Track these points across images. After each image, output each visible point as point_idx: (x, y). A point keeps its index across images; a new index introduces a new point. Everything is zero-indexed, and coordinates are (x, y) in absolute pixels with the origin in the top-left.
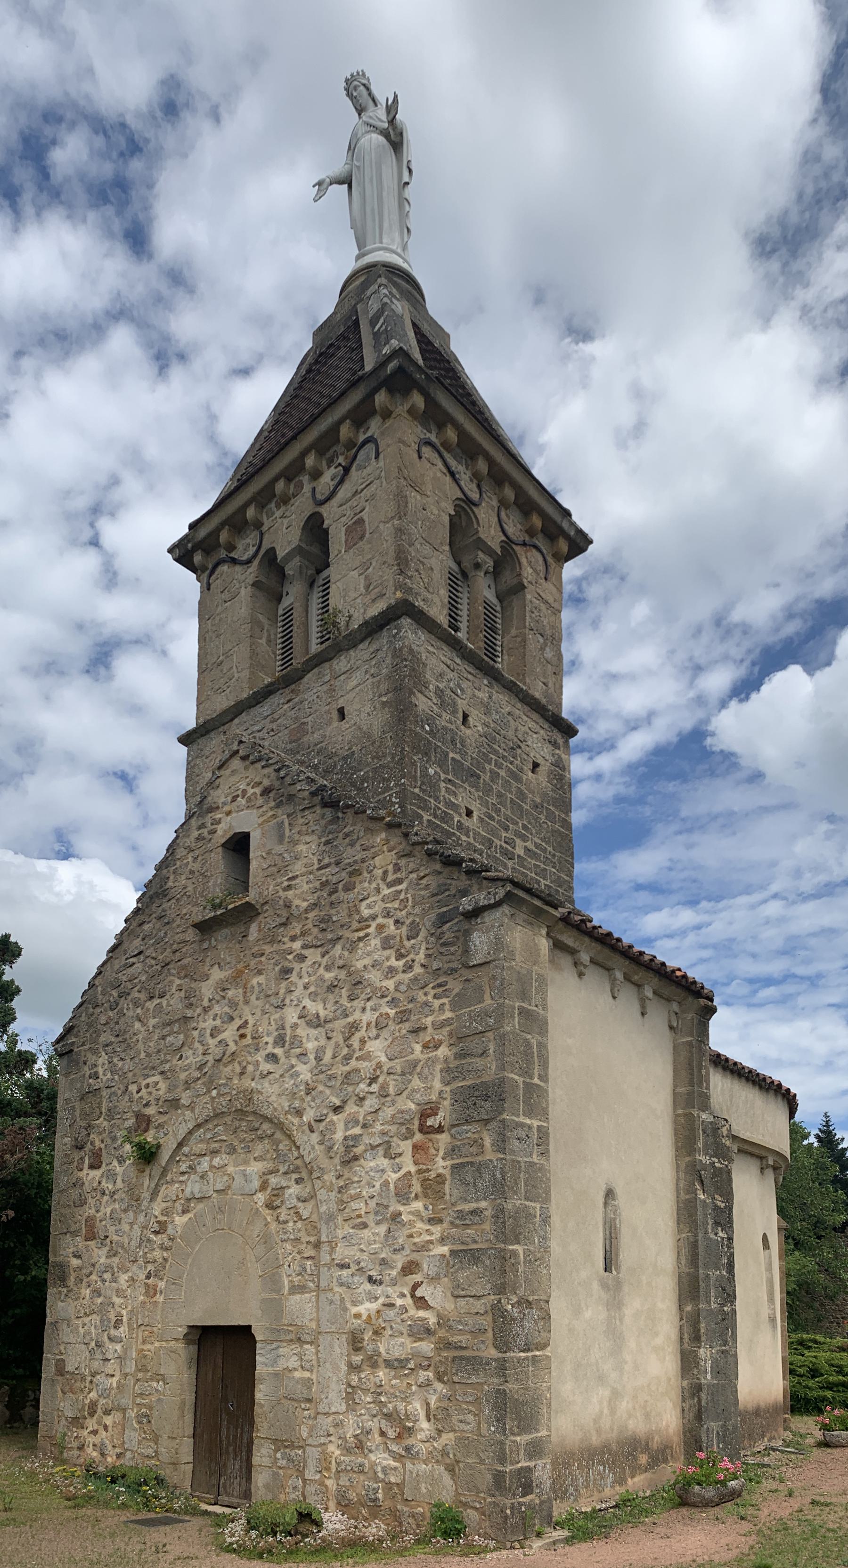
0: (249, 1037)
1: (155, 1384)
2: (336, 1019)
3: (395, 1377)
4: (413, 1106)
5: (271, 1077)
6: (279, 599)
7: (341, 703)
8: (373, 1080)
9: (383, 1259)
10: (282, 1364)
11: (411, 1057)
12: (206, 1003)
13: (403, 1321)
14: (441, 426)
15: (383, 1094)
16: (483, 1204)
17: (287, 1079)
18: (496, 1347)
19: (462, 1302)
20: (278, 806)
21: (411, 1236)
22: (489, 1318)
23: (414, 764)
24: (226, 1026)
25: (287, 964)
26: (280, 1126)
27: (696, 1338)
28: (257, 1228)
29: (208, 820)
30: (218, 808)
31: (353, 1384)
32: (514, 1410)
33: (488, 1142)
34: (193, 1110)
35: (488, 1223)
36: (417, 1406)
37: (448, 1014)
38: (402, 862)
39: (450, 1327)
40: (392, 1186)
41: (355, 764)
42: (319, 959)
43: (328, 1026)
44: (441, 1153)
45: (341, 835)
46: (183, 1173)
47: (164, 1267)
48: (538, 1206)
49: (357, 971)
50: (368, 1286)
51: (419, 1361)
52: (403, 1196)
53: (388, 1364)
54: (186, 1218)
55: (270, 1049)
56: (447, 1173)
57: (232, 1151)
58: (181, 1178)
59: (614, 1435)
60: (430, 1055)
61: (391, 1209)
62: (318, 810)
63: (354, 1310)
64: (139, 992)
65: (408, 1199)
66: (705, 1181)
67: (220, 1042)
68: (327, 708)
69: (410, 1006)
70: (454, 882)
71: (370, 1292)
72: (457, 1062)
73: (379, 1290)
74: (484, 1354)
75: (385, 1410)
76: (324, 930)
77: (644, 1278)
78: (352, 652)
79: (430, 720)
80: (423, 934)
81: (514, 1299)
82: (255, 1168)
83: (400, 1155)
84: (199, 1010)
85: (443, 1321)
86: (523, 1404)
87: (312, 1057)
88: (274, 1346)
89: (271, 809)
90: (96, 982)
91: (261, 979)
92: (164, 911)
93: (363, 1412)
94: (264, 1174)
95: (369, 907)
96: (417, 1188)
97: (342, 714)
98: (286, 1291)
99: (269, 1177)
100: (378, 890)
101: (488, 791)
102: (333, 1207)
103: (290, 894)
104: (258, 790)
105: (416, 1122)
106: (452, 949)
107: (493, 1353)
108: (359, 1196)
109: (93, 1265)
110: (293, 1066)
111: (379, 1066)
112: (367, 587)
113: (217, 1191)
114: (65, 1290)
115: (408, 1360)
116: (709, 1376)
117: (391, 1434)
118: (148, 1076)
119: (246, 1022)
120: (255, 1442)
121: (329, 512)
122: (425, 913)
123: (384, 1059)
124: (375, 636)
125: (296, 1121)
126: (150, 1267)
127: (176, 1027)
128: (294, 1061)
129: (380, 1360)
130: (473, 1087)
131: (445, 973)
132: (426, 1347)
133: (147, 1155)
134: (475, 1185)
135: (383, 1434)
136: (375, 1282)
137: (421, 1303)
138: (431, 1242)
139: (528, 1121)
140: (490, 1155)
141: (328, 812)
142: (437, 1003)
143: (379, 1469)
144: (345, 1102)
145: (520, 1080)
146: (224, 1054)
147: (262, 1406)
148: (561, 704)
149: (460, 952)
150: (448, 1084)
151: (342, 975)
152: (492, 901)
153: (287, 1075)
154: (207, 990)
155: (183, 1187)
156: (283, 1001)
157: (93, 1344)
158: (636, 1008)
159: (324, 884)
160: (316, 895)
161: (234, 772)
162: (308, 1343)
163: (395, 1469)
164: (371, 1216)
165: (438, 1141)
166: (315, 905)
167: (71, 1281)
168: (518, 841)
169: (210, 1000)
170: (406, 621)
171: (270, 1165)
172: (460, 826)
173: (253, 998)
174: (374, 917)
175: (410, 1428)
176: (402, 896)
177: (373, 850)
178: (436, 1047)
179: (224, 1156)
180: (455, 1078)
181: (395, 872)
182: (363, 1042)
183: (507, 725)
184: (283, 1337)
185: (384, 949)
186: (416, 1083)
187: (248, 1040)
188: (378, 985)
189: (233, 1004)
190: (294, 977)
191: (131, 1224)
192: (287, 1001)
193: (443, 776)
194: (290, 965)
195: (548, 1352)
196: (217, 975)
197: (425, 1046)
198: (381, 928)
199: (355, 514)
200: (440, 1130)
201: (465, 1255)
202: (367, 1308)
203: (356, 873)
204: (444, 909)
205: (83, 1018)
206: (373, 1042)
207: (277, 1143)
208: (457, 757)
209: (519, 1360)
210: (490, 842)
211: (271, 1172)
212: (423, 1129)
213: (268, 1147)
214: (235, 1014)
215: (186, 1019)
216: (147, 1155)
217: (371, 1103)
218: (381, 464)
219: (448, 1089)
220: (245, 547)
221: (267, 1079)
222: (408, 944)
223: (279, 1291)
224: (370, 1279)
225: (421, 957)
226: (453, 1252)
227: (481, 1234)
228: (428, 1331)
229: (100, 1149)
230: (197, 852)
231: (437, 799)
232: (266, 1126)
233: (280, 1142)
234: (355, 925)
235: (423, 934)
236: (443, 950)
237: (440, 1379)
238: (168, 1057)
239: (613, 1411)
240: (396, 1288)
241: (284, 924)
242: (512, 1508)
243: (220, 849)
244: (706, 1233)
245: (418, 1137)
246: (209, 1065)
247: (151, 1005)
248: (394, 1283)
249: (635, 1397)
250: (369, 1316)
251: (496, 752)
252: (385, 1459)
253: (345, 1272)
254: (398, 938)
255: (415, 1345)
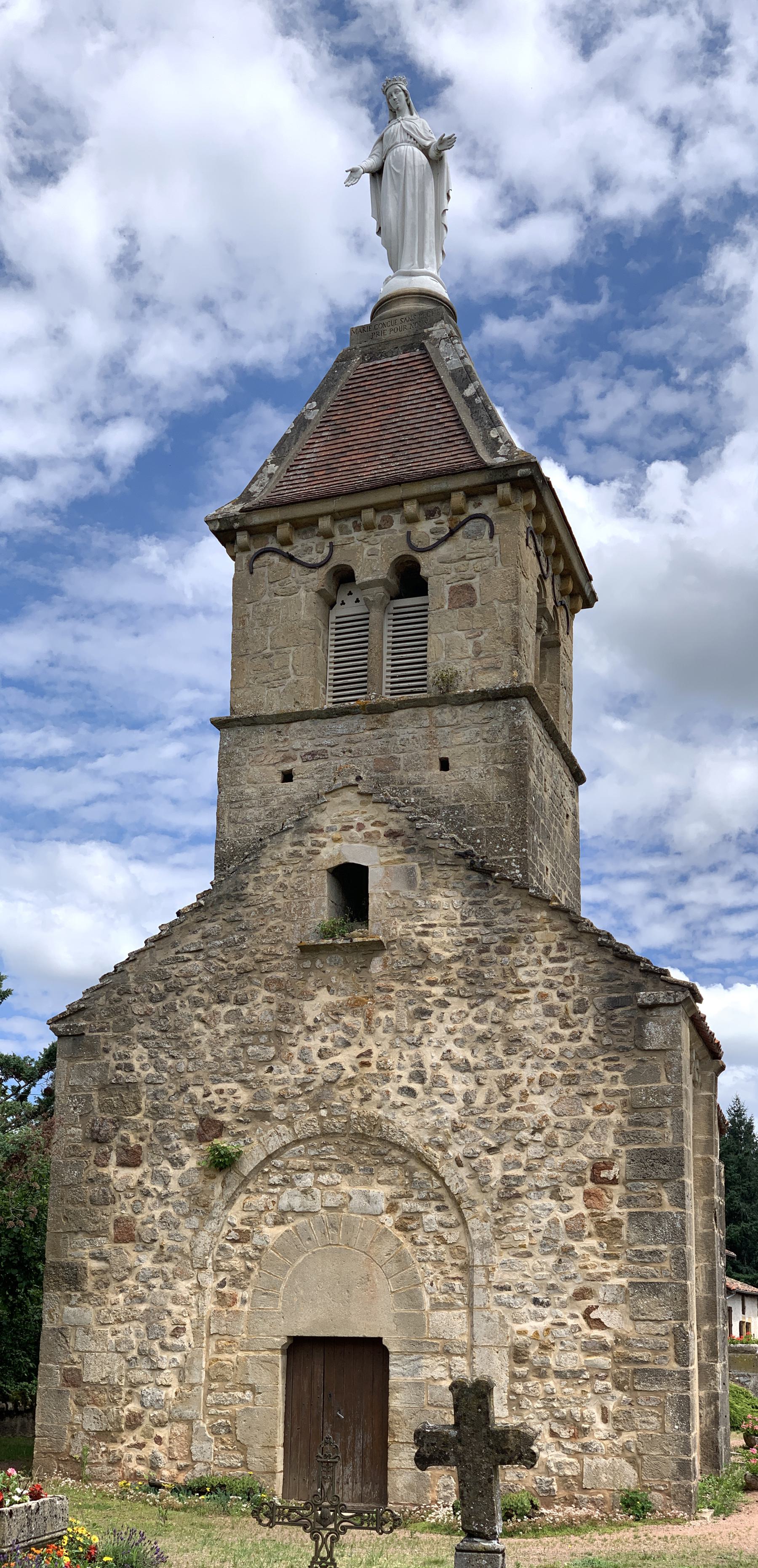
0: (374, 1066)
1: (239, 1394)
2: (489, 1067)
3: (567, 1386)
4: (585, 1159)
5: (405, 1109)
6: (332, 605)
7: (444, 753)
8: (537, 1130)
9: (552, 1285)
10: (425, 1374)
11: (582, 1117)
12: (310, 1022)
13: (575, 1338)
15: (550, 1143)
16: (663, 1247)
17: (427, 1114)
18: (678, 1362)
19: (642, 1325)
20: (408, 852)
21: (586, 1267)
22: (671, 1339)
24: (339, 1050)
25: (424, 1006)
26: (419, 1157)
28: (388, 1245)
29: (308, 838)
30: (322, 831)
31: (518, 1391)
33: (665, 1197)
34: (290, 1124)
35: (667, 1262)
36: (593, 1411)
37: (621, 1086)
38: (568, 944)
39: (630, 1345)
40: (562, 1224)
41: (465, 817)
42: (466, 1009)
43: (478, 1073)
44: (616, 1201)
45: (491, 900)
46: (274, 1185)
47: (248, 1277)
49: (515, 1030)
50: (533, 1308)
51: (595, 1372)
52: (575, 1233)
53: (559, 1374)
54: (280, 1230)
55: (404, 1082)
56: (624, 1219)
57: (347, 1170)
58: (271, 1190)
60: (603, 1118)
61: (561, 1243)
62: (462, 871)
63: (517, 1327)
64: (200, 991)
65: (581, 1236)
67: (333, 1065)
68: (427, 752)
69: (578, 1072)
70: (626, 975)
71: (535, 1312)
72: (632, 1129)
73: (546, 1311)
74: (667, 1367)
75: (557, 1414)
76: (471, 983)
78: (458, 709)
80: (591, 1011)
82: (381, 1192)
83: (570, 1198)
84: (297, 1028)
85: (620, 1340)
87: (460, 1098)
88: (413, 1357)
89: (399, 852)
90: (127, 968)
91: (391, 1014)
92: (237, 915)
93: (531, 1416)
94: (392, 1197)
95: (528, 974)
96: (590, 1227)
97: (445, 765)
98: (427, 1307)
99: (399, 1200)
100: (539, 962)
102: (488, 1235)
103: (427, 940)
104: (382, 830)
105: (589, 1173)
106: (624, 1031)
107: (675, 1366)
108: (522, 1229)
109: (130, 1270)
110: (435, 1103)
111: (545, 1119)
112: (477, 653)
113: (326, 1208)
114: (79, 1294)
115: (582, 1372)
117: (564, 1434)
118: (220, 1081)
119: (369, 1053)
120: (392, 1446)
122: (594, 993)
123: (550, 1113)
124: (488, 703)
125: (439, 1154)
126: (222, 1276)
127: (263, 1039)
128: (436, 1099)
129: (550, 1372)
130: (651, 1152)
131: (616, 1049)
132: (603, 1361)
133: (222, 1164)
134: (654, 1231)
135: (553, 1434)
136: (542, 1304)
137: (598, 1324)
138: (607, 1274)
140: (667, 1208)
141: (476, 877)
142: (608, 1075)
143: (552, 1464)
144: (500, 1145)
146: (339, 1077)
147: (398, 1413)
149: (632, 1034)
150: (624, 1145)
151: (497, 1030)
152: (672, 1002)
153: (428, 1110)
154: (312, 1010)
155: (275, 1198)
156: (420, 1038)
157: (135, 1353)
159: (470, 942)
160: (460, 949)
161: (345, 802)
162: (457, 1355)
163: (571, 1464)
164: (537, 1248)
165: (611, 1191)
166: (460, 958)
167: (89, 1285)
169: (316, 1021)
170: (524, 702)
171: (401, 1190)
173: (380, 1030)
174: (533, 985)
175: (586, 1429)
176: (567, 973)
177: (531, 924)
178: (609, 1112)
179: (335, 1175)
180: (630, 1141)
181: (559, 950)
182: (524, 1095)
184: (426, 1349)
185: (547, 1016)
186: (588, 1139)
187: (373, 1069)
188: (541, 1047)
189: (351, 1031)
190: (432, 1020)
191: (196, 1231)
192: (425, 1040)
194: (429, 1008)
196: (324, 997)
197: (597, 1110)
198: (542, 997)
199: (463, 579)
200: (615, 1181)
201: (645, 1287)
202: (530, 1326)
203: (514, 940)
204: (616, 995)
205: (102, 1001)
206: (537, 1097)
207: (412, 1171)
211: (401, 1197)
212: (595, 1179)
213: (398, 1172)
214: (352, 1041)
215: (279, 1033)
216: (222, 1164)
217: (533, 1151)
218: (496, 544)
219: (623, 1149)
220: (308, 548)
221: (400, 1110)
222: (576, 1017)
223: (420, 1306)
224: (536, 1301)
225: (590, 1030)
226: (631, 1284)
227: (659, 1272)
228: (605, 1348)
229: (139, 1147)
230: (291, 868)
232: (395, 1153)
233: (416, 1170)
234: (511, 987)
235: (591, 1011)
236: (615, 1029)
237: (619, 1387)
238: (252, 1067)
240: (566, 1310)
241: (419, 967)
243: (326, 873)
245: (590, 1185)
246: (316, 1084)
247: (224, 1009)
248: (563, 1305)
250: (537, 1333)
252: (557, 1456)
253: (505, 1294)
254: (564, 1010)
255: (589, 1359)
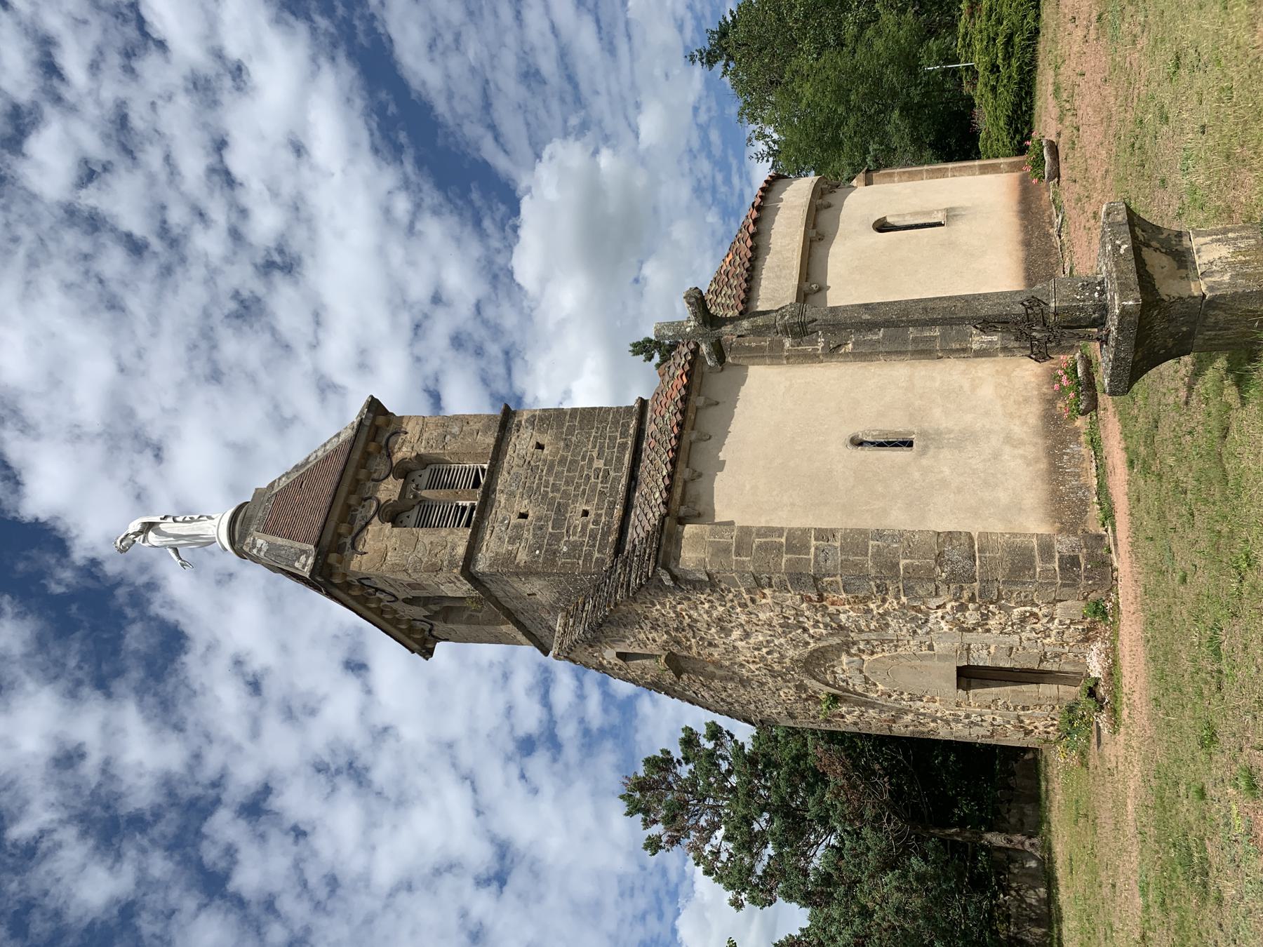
14: (340, 535)
23: (563, 564)
27: (964, 350)
32: (1020, 562)
48: (871, 542)
59: (1040, 441)
66: (838, 342)
77: (917, 403)
79: (531, 550)
81: (938, 569)
86: (1013, 564)
101: (565, 494)
116: (995, 338)
121: (401, 596)
139: (813, 550)
145: (785, 557)
148: (488, 416)
158: (712, 410)
168: (595, 466)
172: (596, 522)
183: (517, 475)
193: (566, 538)
195: (975, 535)
208: (550, 524)
209: (981, 567)
210: (601, 493)
231: (582, 544)
239: (1021, 443)
242: (1087, 578)
244: (878, 341)
249: (1011, 415)
251: (538, 488)
